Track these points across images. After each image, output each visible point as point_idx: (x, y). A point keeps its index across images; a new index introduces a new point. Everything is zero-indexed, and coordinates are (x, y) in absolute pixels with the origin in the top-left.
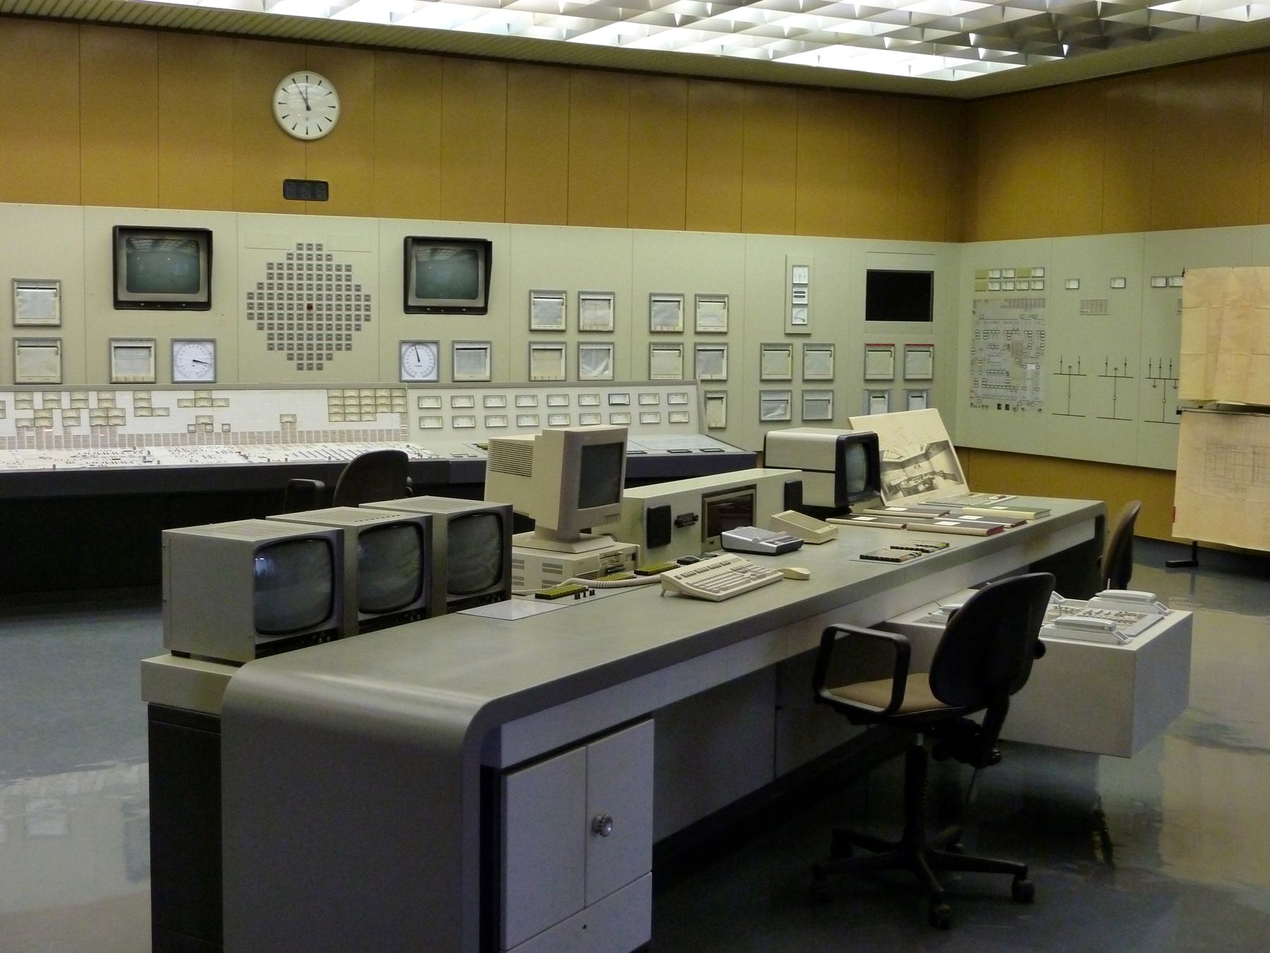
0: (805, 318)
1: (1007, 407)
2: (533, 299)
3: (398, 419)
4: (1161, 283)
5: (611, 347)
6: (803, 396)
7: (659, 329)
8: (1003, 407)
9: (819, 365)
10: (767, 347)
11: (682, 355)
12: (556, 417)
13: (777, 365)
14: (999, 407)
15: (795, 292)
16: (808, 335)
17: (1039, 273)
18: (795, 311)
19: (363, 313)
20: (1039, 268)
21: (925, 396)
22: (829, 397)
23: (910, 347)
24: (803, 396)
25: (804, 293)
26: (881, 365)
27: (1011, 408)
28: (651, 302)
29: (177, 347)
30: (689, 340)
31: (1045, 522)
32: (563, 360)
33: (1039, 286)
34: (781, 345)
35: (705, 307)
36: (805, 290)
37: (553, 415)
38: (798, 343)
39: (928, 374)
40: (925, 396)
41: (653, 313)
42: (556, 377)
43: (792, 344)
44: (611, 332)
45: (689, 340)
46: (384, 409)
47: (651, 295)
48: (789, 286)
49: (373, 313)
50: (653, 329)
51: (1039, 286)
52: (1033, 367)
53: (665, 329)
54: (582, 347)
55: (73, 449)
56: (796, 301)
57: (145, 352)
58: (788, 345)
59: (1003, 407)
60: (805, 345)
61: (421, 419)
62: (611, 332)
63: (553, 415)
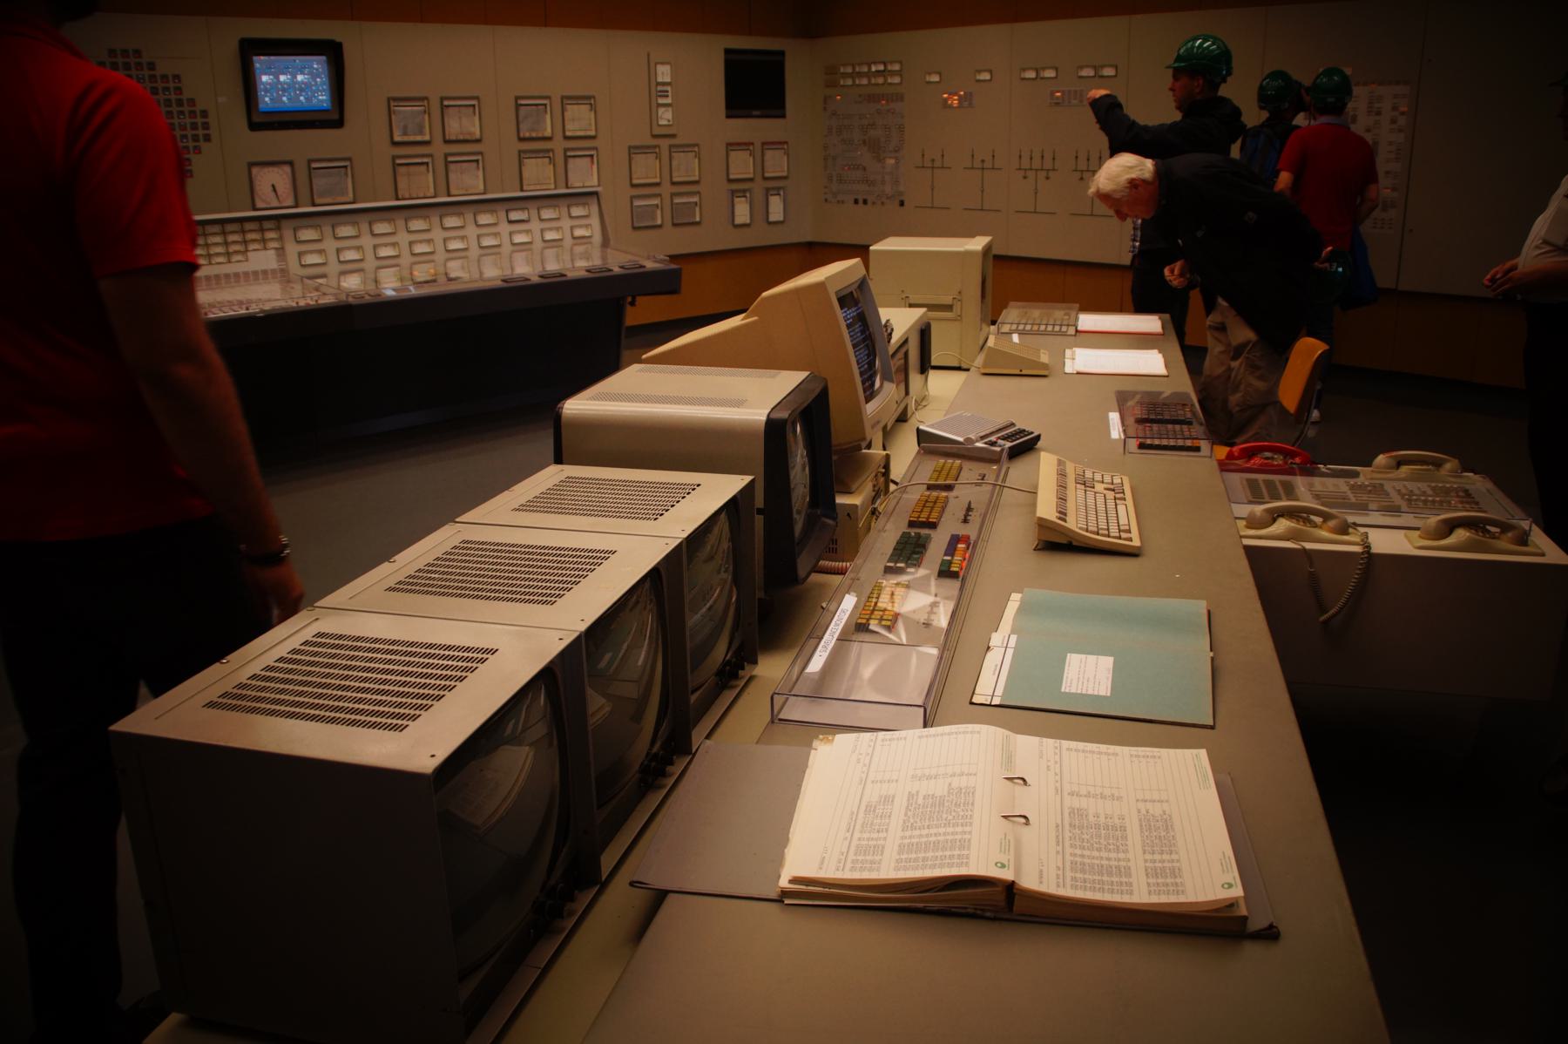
0: (670, 118)
1: (865, 202)
2: (392, 108)
3: (274, 257)
4: (1031, 74)
5: (479, 157)
6: (632, 203)
7: (527, 135)
8: (861, 201)
9: (686, 167)
10: (633, 150)
11: (552, 161)
12: (452, 241)
13: (647, 170)
14: (856, 202)
15: (660, 91)
16: (673, 136)
17: (897, 67)
18: (661, 110)
19: (201, 132)
20: (985, 71)
21: (782, 193)
22: (695, 199)
23: (766, 145)
24: (632, 203)
25: (667, 92)
26: (742, 165)
27: (869, 202)
28: (518, 106)
29: (255, 170)
30: (558, 145)
31: (851, 365)
32: (480, 173)
33: (897, 80)
34: (648, 147)
35: (573, 111)
36: (669, 88)
37: (450, 238)
38: (665, 143)
39: (749, 173)
40: (782, 193)
41: (520, 119)
42: (584, 183)
43: (659, 146)
44: (478, 141)
45: (558, 145)
46: (256, 246)
47: (517, 98)
48: (653, 84)
49: (214, 132)
50: (522, 135)
51: (897, 80)
52: (892, 161)
53: (534, 135)
54: (314, 165)
55: (261, 281)
56: (661, 101)
57: (423, 168)
58: (655, 147)
59: (861, 201)
60: (670, 146)
61: (300, 254)
62: (478, 141)
63: (450, 238)
